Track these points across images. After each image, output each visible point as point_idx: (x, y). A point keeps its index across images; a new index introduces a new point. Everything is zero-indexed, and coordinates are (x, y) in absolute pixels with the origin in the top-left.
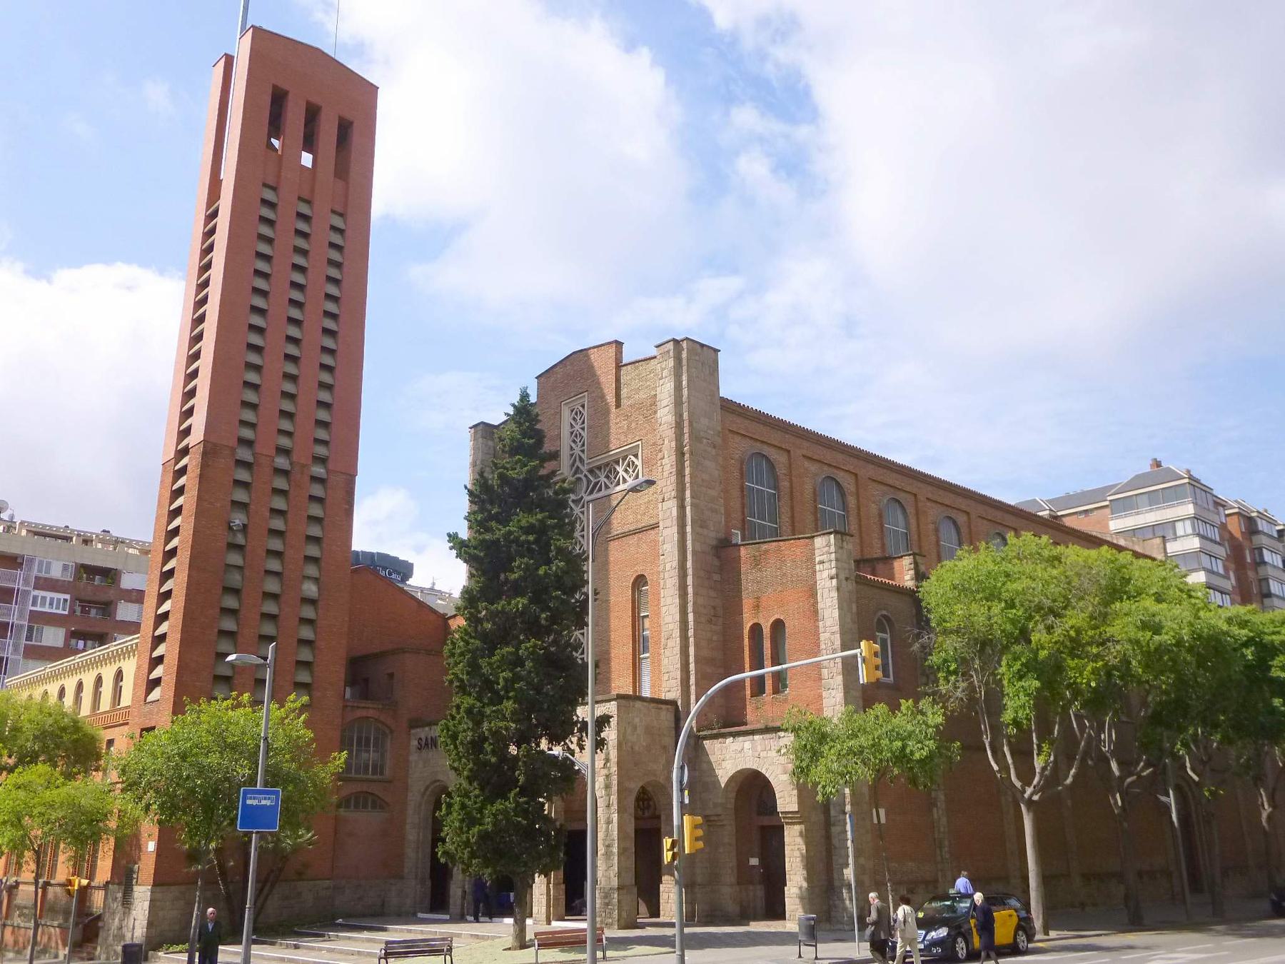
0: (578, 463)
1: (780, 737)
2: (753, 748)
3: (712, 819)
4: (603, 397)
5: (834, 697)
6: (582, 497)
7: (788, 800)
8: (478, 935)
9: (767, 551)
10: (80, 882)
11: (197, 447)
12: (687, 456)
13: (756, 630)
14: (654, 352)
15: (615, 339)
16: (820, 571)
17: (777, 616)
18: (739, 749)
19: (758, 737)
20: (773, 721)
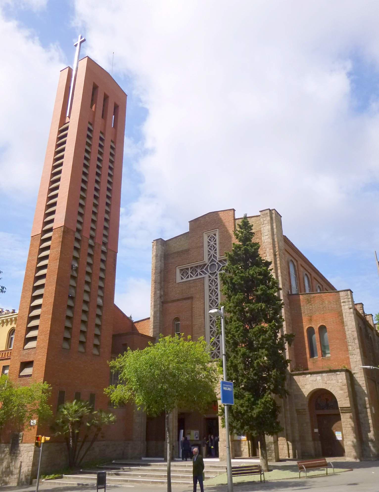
0: (212, 257)
1: (337, 374)
2: (323, 379)
3: (300, 411)
4: (227, 231)
5: (356, 358)
6: (216, 272)
7: (344, 402)
8: (215, 466)
9: (314, 297)
10: (45, 439)
11: (58, 228)
12: (278, 256)
13: (311, 331)
14: (259, 214)
15: (233, 208)
16: (343, 306)
17: (321, 324)
18: (315, 380)
19: (325, 374)
20: (323, 368)
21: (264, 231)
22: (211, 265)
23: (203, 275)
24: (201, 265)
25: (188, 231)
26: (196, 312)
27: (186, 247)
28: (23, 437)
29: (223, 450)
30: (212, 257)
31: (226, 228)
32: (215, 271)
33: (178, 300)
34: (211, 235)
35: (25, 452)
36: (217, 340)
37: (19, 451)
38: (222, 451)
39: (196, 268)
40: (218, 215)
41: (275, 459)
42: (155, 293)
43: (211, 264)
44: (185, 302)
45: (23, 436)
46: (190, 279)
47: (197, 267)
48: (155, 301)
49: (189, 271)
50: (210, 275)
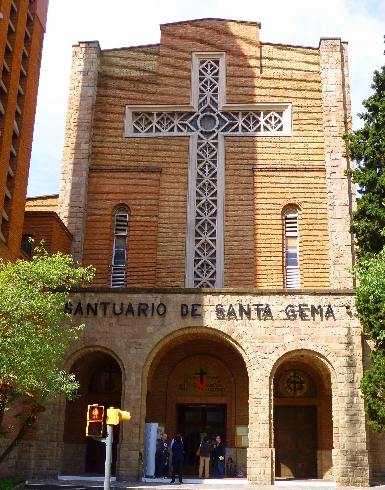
0: (208, 103)
21: (328, 76)
22: (203, 117)
23: (186, 133)
24: (182, 114)
26: (167, 199)
29: (260, 463)
30: (208, 103)
31: (243, 55)
32: (211, 130)
33: (128, 170)
34: (208, 61)
38: (258, 465)
39: (169, 117)
40: (227, 27)
41: (369, 481)
42: (77, 147)
44: (143, 175)
46: (154, 133)
47: (172, 114)
49: (153, 120)
50: (201, 135)
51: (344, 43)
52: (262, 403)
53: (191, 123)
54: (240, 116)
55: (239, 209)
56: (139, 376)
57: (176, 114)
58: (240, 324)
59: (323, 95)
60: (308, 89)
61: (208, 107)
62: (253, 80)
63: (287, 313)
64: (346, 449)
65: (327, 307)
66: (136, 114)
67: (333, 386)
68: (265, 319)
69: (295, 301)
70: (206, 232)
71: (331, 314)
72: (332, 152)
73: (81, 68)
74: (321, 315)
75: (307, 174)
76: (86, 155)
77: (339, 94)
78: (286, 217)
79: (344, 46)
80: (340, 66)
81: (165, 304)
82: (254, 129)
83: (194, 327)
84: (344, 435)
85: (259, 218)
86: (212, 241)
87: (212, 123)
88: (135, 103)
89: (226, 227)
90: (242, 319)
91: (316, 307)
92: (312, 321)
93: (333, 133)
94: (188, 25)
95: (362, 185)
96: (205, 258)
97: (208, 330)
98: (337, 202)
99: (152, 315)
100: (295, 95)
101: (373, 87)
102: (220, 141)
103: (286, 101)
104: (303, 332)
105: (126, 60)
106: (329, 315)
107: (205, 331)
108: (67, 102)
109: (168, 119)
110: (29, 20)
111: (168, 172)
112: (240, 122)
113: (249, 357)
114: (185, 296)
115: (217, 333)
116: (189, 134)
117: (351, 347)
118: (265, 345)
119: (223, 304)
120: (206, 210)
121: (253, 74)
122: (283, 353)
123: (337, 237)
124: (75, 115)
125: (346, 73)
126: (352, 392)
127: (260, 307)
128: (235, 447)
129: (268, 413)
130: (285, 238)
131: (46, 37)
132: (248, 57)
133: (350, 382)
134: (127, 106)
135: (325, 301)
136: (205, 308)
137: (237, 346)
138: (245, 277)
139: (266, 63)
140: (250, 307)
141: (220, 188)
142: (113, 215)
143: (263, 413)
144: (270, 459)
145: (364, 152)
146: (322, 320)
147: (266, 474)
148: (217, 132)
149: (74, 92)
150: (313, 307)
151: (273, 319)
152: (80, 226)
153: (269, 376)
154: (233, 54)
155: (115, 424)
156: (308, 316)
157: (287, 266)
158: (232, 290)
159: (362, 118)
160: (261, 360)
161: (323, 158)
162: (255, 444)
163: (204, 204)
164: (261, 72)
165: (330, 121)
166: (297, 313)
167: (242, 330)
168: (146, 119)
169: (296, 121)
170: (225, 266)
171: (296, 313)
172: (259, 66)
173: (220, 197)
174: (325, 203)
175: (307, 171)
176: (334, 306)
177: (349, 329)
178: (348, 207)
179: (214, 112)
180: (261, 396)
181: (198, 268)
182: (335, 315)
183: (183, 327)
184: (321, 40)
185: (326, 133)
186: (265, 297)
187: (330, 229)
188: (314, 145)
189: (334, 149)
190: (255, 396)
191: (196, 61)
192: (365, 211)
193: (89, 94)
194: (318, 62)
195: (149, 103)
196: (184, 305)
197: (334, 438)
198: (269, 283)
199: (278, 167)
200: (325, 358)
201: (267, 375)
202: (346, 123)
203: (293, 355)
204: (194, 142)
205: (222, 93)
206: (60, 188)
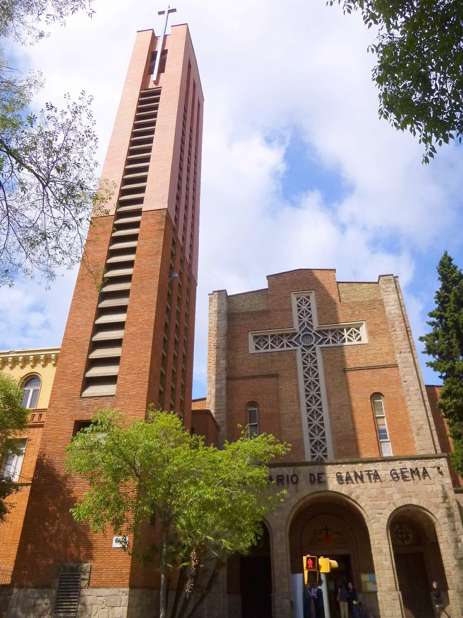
11: (155, 212)
21: (390, 300)
23: (292, 348)
24: (289, 335)
25: (267, 287)
26: (284, 396)
27: (262, 307)
28: (90, 573)
32: (311, 344)
33: (254, 377)
34: (302, 297)
35: (100, 607)
36: (321, 438)
37: (84, 604)
39: (280, 337)
42: (218, 363)
43: (304, 333)
44: (266, 380)
45: (91, 571)
46: (270, 350)
47: (282, 335)
48: (218, 375)
49: (268, 340)
50: (303, 348)
51: (396, 277)
52: (384, 551)
53: (295, 340)
54: (330, 333)
55: (338, 399)
56: (283, 534)
57: (284, 335)
58: (356, 487)
59: (387, 313)
60: (375, 310)
61: (306, 328)
62: (336, 307)
63: (392, 475)
64: (460, 589)
65: (422, 469)
66: (256, 337)
67: (438, 534)
68: (375, 482)
69: (397, 466)
70: (315, 418)
71: (427, 475)
72: (401, 353)
73: (216, 309)
74: (419, 476)
75: (384, 370)
76: (224, 368)
77: (398, 312)
78: (374, 402)
79: (396, 279)
80: (396, 293)
81: (296, 474)
82: (341, 341)
83: (321, 491)
84: (456, 576)
85: (354, 404)
86: (321, 424)
87: (310, 339)
88: (255, 330)
89: (330, 413)
90: (357, 483)
91: (414, 470)
92: (412, 481)
93: (399, 339)
94: (286, 274)
95: (442, 372)
96: (317, 438)
97: (331, 493)
98: (411, 388)
99: (288, 483)
100: (366, 315)
101: (436, 302)
102: (318, 352)
103: (361, 319)
104: (407, 491)
105: (245, 301)
106: (425, 476)
107: (329, 494)
108: (208, 332)
109: (279, 339)
110: (188, 278)
111: (283, 376)
112: (330, 337)
113: (367, 513)
114: (311, 467)
115: (339, 495)
116: (295, 348)
117: (447, 500)
118: (378, 503)
119: (340, 472)
120: (314, 401)
121: (335, 304)
122: (394, 508)
123: (415, 415)
124: (214, 341)
125: (401, 297)
126: (456, 539)
127: (370, 472)
128: (362, 592)
129: (390, 559)
130: (375, 419)
131: (198, 288)
132: (330, 292)
133: (452, 530)
134: (249, 332)
135: (420, 464)
136: (328, 475)
137: (356, 505)
138: (350, 450)
139: (342, 296)
140: (362, 473)
141: (322, 385)
142: (246, 410)
143: (386, 560)
144: (398, 601)
145: (439, 348)
146: (420, 479)
147: (397, 615)
148: (315, 345)
149: (212, 325)
150: (411, 469)
151: (381, 481)
152: (224, 419)
153: (386, 528)
154: (320, 291)
155: (327, 572)
156: (408, 477)
157: (380, 439)
158: (347, 460)
159: (430, 324)
160: (377, 516)
161: (394, 357)
162: (384, 588)
163: (311, 398)
164: (340, 302)
165: (396, 331)
166: (400, 475)
167: (358, 491)
168: (264, 340)
169: (371, 333)
170: (333, 443)
171: (399, 475)
172: (338, 298)
173: (323, 392)
174: (401, 390)
175: (384, 368)
176: (428, 467)
177: (443, 486)
178: (420, 391)
179: (311, 332)
180: (382, 546)
181: (313, 446)
182: (430, 475)
183: (313, 492)
184: (380, 276)
185: (394, 339)
186: (372, 464)
187: (410, 408)
188: (386, 349)
189: (402, 350)
190: (377, 546)
191: (294, 298)
192: (451, 391)
193: (223, 326)
194: (380, 291)
195: (265, 329)
196: (311, 475)
197: (448, 581)
198: (369, 453)
199: (362, 366)
200: (428, 511)
201: (383, 527)
202: (407, 331)
203: (402, 509)
204: (299, 354)
205: (315, 318)
206: (207, 392)
